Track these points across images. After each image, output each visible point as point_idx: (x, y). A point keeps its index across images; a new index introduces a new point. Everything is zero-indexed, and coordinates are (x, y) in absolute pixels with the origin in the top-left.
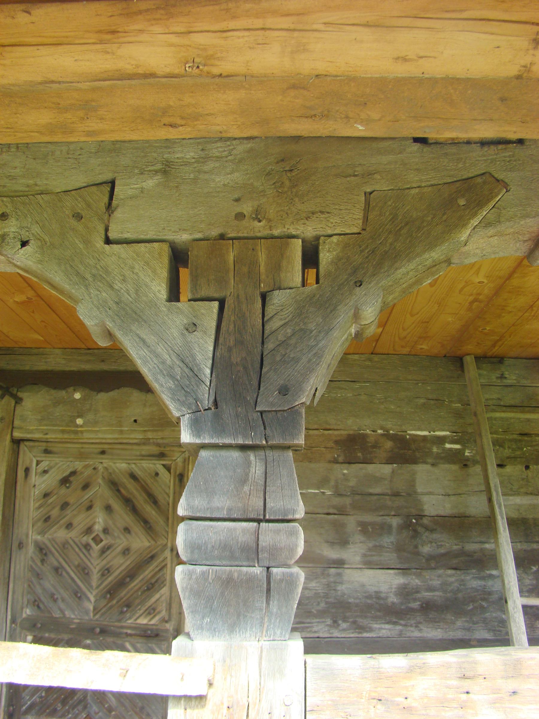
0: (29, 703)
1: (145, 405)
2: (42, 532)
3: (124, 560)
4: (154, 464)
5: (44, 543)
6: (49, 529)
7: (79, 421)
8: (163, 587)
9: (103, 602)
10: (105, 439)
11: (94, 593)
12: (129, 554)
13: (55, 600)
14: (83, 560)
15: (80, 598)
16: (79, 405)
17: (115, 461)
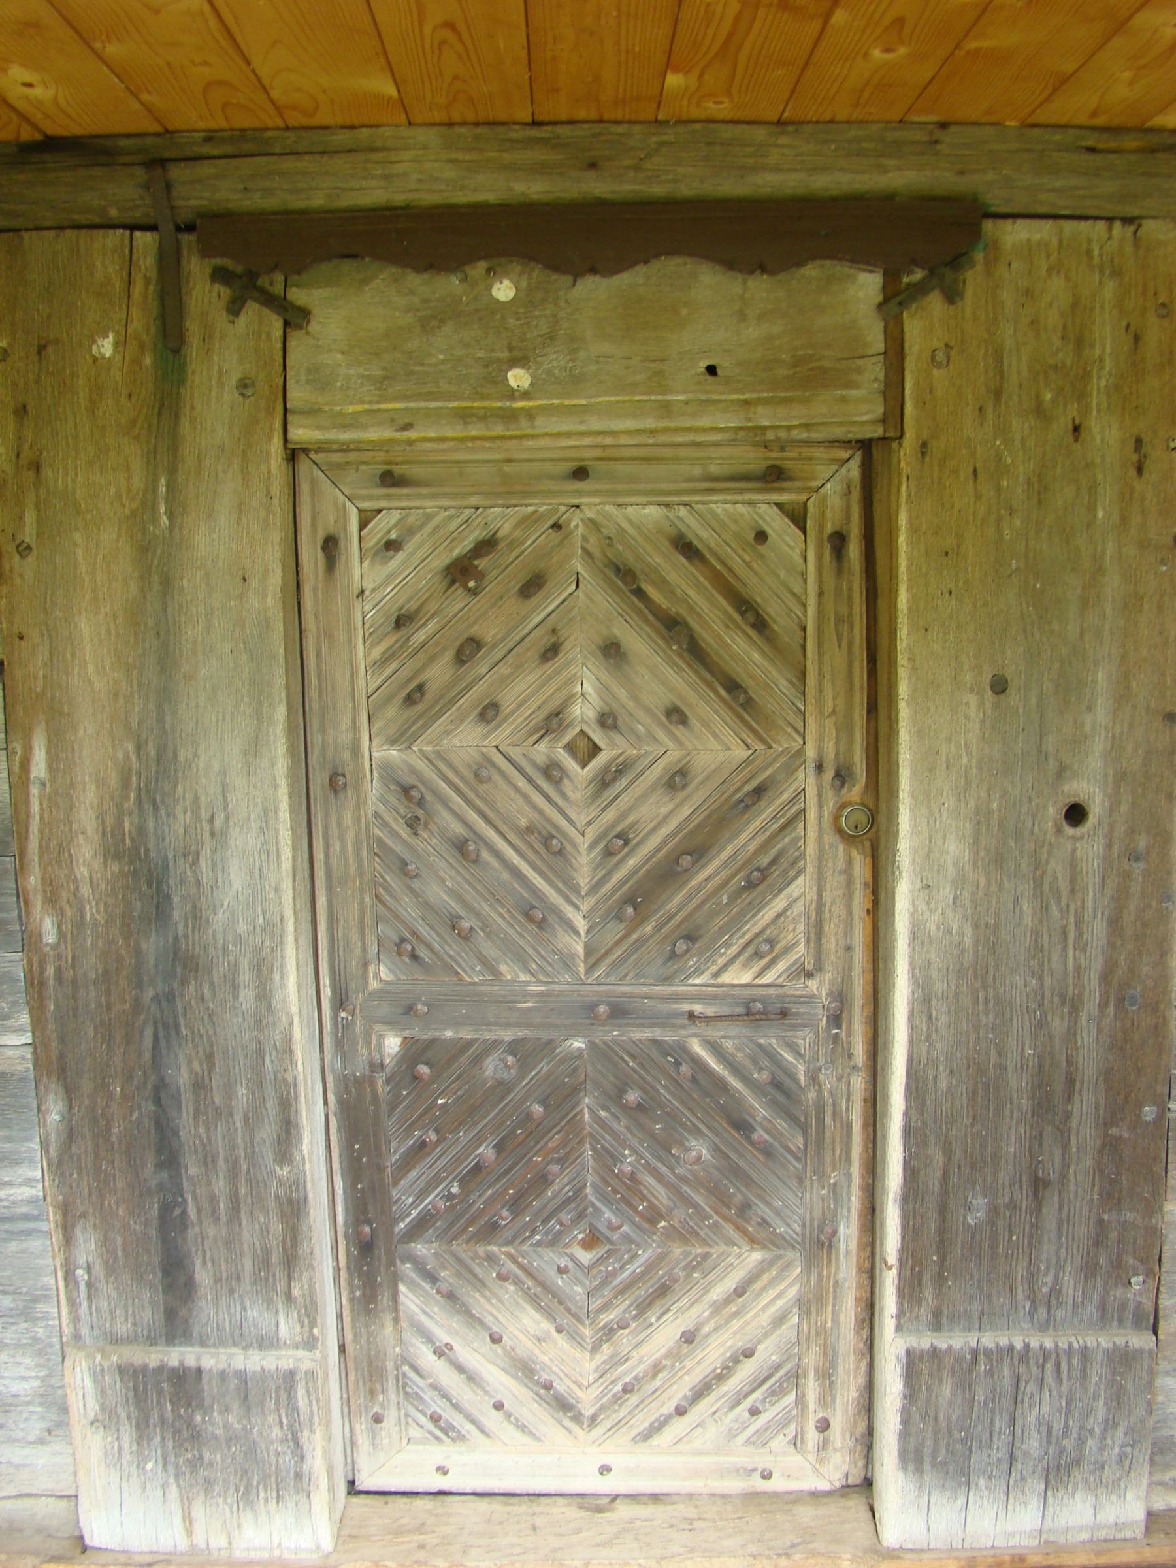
0: (414, 1213)
1: (742, 317)
2: (403, 737)
3: (671, 806)
4: (751, 503)
5: (413, 771)
6: (426, 727)
7: (518, 378)
8: (796, 878)
9: (615, 931)
10: (612, 433)
11: (585, 907)
12: (684, 787)
13: (466, 937)
14: (541, 812)
15: (542, 924)
16: (512, 322)
17: (621, 500)
